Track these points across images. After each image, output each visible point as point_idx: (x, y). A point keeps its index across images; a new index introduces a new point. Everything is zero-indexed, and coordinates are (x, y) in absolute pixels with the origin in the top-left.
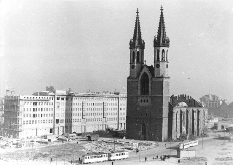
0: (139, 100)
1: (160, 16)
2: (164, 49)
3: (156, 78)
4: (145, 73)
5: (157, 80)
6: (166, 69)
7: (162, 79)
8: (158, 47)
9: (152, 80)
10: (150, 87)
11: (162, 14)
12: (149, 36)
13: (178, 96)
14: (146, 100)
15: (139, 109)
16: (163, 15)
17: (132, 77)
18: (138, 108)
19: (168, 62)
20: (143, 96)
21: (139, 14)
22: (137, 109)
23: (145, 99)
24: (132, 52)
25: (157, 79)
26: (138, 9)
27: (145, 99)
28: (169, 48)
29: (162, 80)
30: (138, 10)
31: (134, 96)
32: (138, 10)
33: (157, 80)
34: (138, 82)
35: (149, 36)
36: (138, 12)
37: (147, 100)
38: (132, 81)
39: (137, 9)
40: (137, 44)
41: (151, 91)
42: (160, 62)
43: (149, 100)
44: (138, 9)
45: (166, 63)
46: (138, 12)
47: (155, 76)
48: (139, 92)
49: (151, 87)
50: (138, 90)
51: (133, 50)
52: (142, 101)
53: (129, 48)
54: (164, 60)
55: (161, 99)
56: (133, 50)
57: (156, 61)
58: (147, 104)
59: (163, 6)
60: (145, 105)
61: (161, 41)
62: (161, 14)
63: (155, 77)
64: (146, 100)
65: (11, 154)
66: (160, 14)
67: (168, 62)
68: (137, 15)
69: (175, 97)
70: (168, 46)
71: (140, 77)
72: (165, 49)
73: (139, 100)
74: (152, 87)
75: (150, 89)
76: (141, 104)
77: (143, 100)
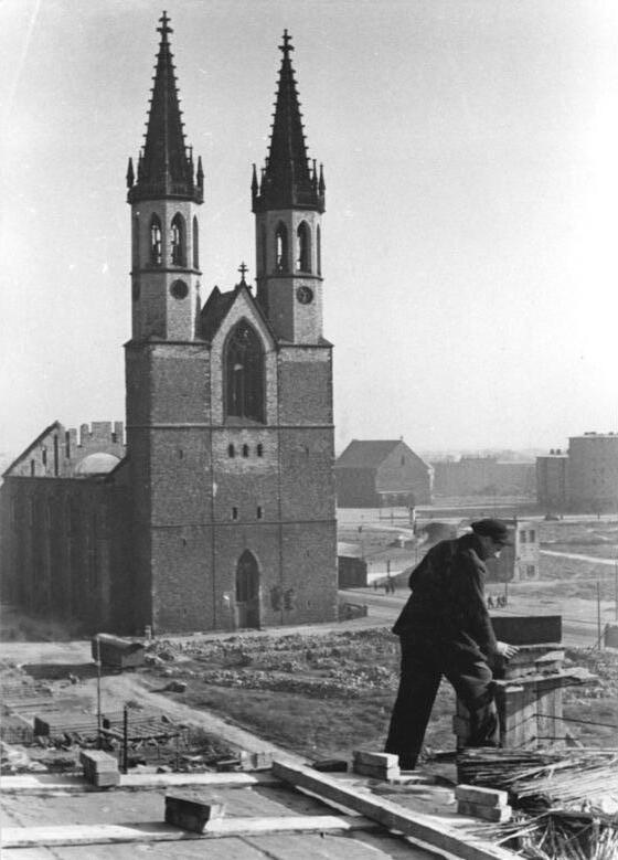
0: (222, 442)
1: (155, 61)
2: (182, 212)
3: (296, 346)
5: (307, 356)
7: (326, 353)
8: (155, 198)
10: (269, 387)
11: (290, 66)
12: (228, 145)
13: (83, 427)
14: (252, 444)
16: (170, 56)
17: (175, 339)
18: (215, 486)
19: (200, 274)
20: (240, 429)
21: (292, 55)
22: (211, 489)
23: (249, 445)
25: (302, 351)
27: (247, 438)
28: (203, 206)
30: (164, 20)
31: (188, 428)
33: (307, 356)
35: (228, 145)
39: (161, 15)
40: (164, 174)
41: (275, 404)
42: (293, 277)
44: (286, 31)
46: (165, 31)
47: (296, 339)
48: (217, 411)
49: (275, 387)
51: (149, 207)
52: (231, 451)
53: (125, 198)
54: (310, 271)
57: (142, 266)
58: (261, 461)
59: (168, 16)
60: (252, 468)
61: (288, 184)
62: (162, 50)
63: (296, 343)
64: (252, 444)
66: (157, 50)
67: (200, 274)
69: (67, 434)
71: (219, 340)
72: (194, 208)
74: (279, 390)
75: (271, 394)
77: (237, 445)
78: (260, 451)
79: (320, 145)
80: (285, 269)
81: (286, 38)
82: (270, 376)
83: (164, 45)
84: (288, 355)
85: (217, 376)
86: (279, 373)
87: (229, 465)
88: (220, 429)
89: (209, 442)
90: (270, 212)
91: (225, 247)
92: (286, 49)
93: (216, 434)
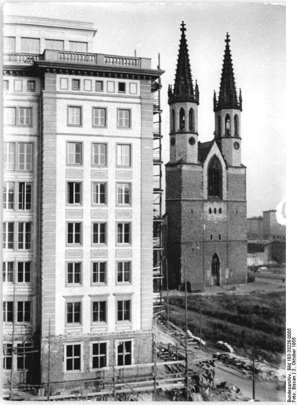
0: (206, 209)
4: (215, 157)
5: (236, 171)
6: (234, 151)
9: (228, 171)
15: (206, 227)
18: (204, 226)
24: (178, 111)
26: (183, 22)
27: (216, 205)
29: (244, 173)
32: (183, 25)
33: (236, 171)
34: (202, 172)
36: (185, 29)
37: (220, 209)
38: (191, 170)
39: (182, 23)
43: (224, 209)
44: (183, 22)
45: (234, 140)
48: (205, 195)
50: (202, 189)
52: (210, 211)
55: (243, 206)
56: (227, 112)
59: (184, 23)
60: (217, 218)
61: (228, 99)
65: (78, 399)
68: (227, 47)
70: (240, 108)
73: (206, 209)
76: (209, 216)
78: (220, 211)
79: (241, 83)
80: (226, 133)
81: (228, 36)
82: (224, 180)
83: (227, 47)
84: (231, 171)
85: (206, 179)
86: (227, 178)
87: (211, 217)
88: (206, 201)
89: (203, 207)
90: (223, 110)
91: (205, 129)
92: (227, 41)
93: (205, 203)
